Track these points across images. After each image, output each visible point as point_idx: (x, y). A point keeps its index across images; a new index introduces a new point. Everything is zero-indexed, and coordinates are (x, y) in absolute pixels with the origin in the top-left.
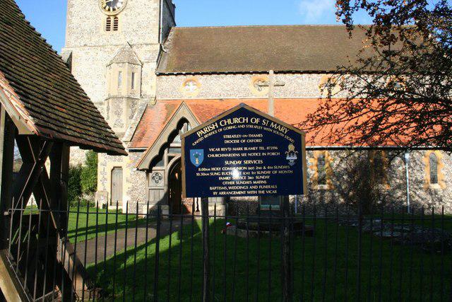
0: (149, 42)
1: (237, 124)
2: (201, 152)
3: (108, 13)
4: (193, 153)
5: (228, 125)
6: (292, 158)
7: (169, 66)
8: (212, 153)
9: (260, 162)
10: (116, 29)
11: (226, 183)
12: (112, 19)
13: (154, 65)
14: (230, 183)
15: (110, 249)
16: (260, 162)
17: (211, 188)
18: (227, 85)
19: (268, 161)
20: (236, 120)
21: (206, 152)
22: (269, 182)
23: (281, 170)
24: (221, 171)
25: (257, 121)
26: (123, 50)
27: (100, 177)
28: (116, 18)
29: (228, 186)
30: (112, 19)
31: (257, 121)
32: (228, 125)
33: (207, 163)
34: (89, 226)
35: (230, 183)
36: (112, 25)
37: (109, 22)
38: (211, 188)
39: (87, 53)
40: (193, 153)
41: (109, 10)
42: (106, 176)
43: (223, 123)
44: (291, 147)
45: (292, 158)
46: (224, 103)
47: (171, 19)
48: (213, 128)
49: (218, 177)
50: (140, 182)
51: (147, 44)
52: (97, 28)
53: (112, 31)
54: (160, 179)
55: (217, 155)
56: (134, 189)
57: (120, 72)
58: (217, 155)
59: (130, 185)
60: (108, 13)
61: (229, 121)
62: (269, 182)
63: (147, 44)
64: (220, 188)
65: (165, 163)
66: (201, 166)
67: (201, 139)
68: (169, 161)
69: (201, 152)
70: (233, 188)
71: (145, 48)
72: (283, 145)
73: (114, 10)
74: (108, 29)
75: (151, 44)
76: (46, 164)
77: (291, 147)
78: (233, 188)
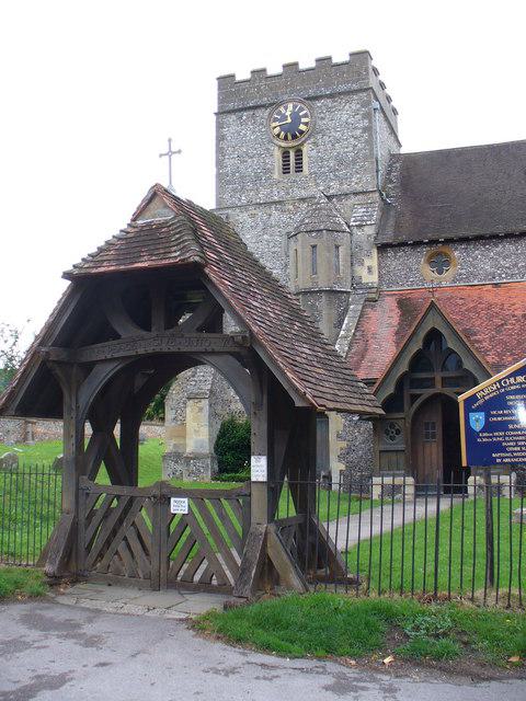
0: (359, 188)
1: (521, 384)
2: (481, 416)
3: (283, 144)
4: (473, 416)
5: (511, 385)
8: (494, 416)
10: (299, 169)
11: (511, 449)
12: (292, 154)
13: (370, 231)
14: (516, 449)
17: (494, 455)
21: (488, 416)
24: (505, 436)
28: (299, 153)
29: (512, 452)
30: (292, 154)
32: (511, 385)
34: (167, 157)
35: (516, 449)
36: (292, 161)
37: (286, 155)
38: (494, 455)
39: (253, 216)
40: (473, 416)
41: (286, 138)
43: (505, 382)
48: (495, 388)
49: (500, 442)
50: (360, 438)
54: (398, 432)
55: (499, 419)
56: (349, 450)
57: (314, 247)
58: (499, 419)
59: (344, 444)
60: (283, 144)
61: (512, 380)
64: (502, 455)
65: (406, 407)
67: (481, 402)
68: (412, 403)
69: (481, 416)
70: (519, 454)
71: (353, 200)
73: (294, 137)
74: (286, 170)
76: (47, 616)
78: (519, 454)
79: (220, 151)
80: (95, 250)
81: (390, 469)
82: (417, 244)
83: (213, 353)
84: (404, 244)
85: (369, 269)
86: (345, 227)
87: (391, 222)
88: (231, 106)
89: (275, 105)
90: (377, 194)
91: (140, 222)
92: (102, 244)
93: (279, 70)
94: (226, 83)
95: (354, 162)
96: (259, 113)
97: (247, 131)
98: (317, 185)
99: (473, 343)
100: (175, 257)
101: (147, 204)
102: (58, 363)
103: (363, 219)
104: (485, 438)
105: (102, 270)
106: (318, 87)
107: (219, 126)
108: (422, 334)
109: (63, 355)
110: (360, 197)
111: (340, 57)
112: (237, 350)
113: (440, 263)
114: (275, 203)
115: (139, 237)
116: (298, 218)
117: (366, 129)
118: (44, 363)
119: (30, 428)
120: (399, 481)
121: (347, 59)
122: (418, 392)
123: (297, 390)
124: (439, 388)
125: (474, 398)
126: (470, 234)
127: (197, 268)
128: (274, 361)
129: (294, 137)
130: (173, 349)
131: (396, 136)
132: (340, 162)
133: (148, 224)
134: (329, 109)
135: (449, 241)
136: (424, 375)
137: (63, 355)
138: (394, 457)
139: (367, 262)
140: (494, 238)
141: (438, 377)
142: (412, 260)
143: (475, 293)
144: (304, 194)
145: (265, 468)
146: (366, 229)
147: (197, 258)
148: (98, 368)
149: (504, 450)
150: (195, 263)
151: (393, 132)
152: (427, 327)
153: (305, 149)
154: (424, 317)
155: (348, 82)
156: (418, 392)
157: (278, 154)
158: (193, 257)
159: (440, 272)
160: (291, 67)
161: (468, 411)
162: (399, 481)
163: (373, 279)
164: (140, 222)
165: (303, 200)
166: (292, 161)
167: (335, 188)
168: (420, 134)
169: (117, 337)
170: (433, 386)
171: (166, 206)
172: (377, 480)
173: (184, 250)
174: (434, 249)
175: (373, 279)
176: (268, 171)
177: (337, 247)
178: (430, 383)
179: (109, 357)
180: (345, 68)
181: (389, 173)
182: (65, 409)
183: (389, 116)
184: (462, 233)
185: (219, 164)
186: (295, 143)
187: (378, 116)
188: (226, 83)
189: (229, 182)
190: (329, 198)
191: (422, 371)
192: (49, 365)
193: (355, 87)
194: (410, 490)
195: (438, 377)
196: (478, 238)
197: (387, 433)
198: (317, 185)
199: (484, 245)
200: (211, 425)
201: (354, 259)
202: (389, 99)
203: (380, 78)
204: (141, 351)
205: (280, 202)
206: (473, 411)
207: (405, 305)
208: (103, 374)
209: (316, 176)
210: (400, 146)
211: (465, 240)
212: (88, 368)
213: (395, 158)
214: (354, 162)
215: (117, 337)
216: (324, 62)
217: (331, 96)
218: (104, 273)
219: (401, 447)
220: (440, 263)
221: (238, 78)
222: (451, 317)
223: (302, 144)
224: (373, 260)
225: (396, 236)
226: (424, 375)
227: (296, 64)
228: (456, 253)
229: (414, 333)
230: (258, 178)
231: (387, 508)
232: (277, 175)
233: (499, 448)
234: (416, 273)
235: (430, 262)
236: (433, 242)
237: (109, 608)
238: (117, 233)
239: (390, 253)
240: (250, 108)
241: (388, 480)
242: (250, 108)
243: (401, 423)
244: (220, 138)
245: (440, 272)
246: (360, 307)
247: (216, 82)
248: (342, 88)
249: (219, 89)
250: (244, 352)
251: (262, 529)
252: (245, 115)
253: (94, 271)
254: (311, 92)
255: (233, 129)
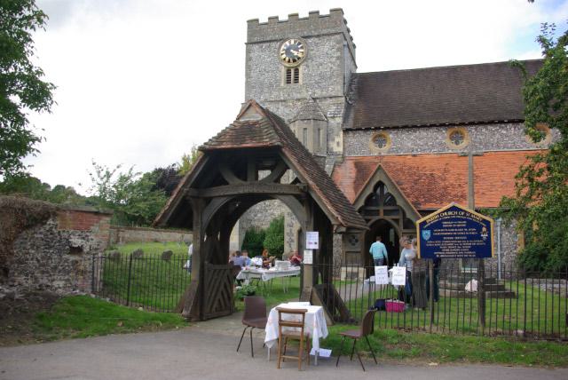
2: (428, 232)
3: (288, 65)
4: (424, 232)
6: (484, 236)
7: (356, 120)
9: (465, 238)
10: (296, 80)
12: (293, 71)
13: (339, 120)
15: (353, 295)
16: (465, 238)
18: (420, 139)
19: (470, 238)
20: (450, 213)
22: (470, 250)
23: (479, 243)
25: (463, 213)
26: (306, 108)
27: (287, 238)
28: (297, 71)
30: (293, 71)
31: (463, 213)
33: (433, 238)
36: (292, 76)
37: (289, 72)
40: (424, 232)
41: (289, 61)
42: (293, 238)
44: (484, 229)
45: (484, 236)
46: (417, 159)
47: (352, 63)
51: (331, 98)
52: (277, 81)
53: (292, 85)
54: (357, 241)
57: (305, 129)
62: (470, 250)
63: (331, 98)
66: (430, 240)
69: (428, 232)
71: (329, 101)
72: (479, 228)
73: (294, 61)
74: (288, 82)
75: (335, 97)
77: (484, 229)
79: (248, 68)
80: (216, 135)
81: (352, 263)
82: (367, 129)
83: (283, 194)
84: (360, 129)
85: (338, 143)
86: (324, 118)
87: (352, 115)
88: (256, 39)
89: (282, 40)
90: (344, 99)
91: (241, 120)
92: (220, 131)
93: (286, 18)
94: (253, 24)
95: (330, 78)
96: (273, 44)
97: (263, 55)
98: (307, 91)
99: (402, 189)
100: (266, 142)
101: (246, 111)
102: (193, 197)
103: (334, 112)
104: (430, 244)
105: (223, 147)
106: (310, 30)
107: (248, 52)
108: (373, 184)
109: (194, 192)
110: (334, 99)
111: (325, 11)
112: (298, 193)
113: (380, 141)
114: (282, 101)
115: (241, 129)
116: (295, 111)
117: (338, 58)
118: (184, 197)
119: (121, 234)
120: (355, 270)
121: (328, 13)
122: (369, 217)
123: (333, 216)
124: (381, 216)
125: (425, 223)
126: (400, 125)
127: (278, 148)
128: (320, 199)
129: (294, 61)
130: (261, 191)
131: (355, 62)
132: (322, 76)
133: (247, 122)
134: (317, 45)
135: (386, 128)
136: (373, 208)
137: (194, 192)
138: (354, 255)
139: (337, 140)
140: (415, 127)
141: (381, 209)
142: (364, 139)
143: (401, 160)
144: (299, 96)
145: (311, 257)
146: (337, 119)
147: (279, 143)
148: (214, 200)
149: (441, 250)
150: (278, 146)
151: (353, 59)
152: (376, 180)
153: (301, 69)
154: (375, 174)
155: (328, 28)
156: (369, 217)
157: (284, 71)
158: (276, 142)
159: (380, 146)
160: (294, 16)
161: (421, 229)
162: (355, 270)
163: (340, 149)
164: (241, 120)
165: (299, 100)
166: (292, 76)
167: (318, 93)
168: (367, 63)
169: (227, 183)
170: (378, 214)
171: (257, 112)
172: (343, 269)
173: (271, 138)
174: (378, 132)
175: (340, 149)
176: (277, 81)
177: (319, 130)
178: (377, 212)
179: (222, 194)
180: (327, 19)
181: (350, 85)
182: (194, 225)
183: (350, 47)
184: (395, 124)
185: (248, 75)
186: (295, 65)
187: (346, 49)
188: (253, 24)
189: (253, 87)
190: (314, 99)
191: (371, 205)
192: (188, 198)
193: (333, 31)
194: (361, 275)
195: (381, 209)
196: (404, 127)
197: (350, 241)
198: (307, 91)
199: (408, 131)
200: (240, 235)
201: (328, 138)
202: (351, 39)
203: (348, 25)
204: (241, 192)
205: (284, 101)
206: (425, 229)
207: (360, 166)
208: (217, 204)
209: (307, 86)
210: (356, 67)
211: (396, 128)
212: (208, 200)
213: (354, 75)
214: (330, 78)
215: (227, 183)
216: (314, 14)
217: (318, 36)
218: (224, 149)
219: (359, 250)
220: (380, 141)
221: (260, 22)
222: (390, 175)
223: (299, 66)
224: (340, 138)
225: (355, 124)
226: (373, 208)
227: (297, 15)
228: (391, 136)
229: (369, 183)
230: (271, 85)
231: (348, 285)
232: (283, 84)
233: (438, 249)
234: (367, 147)
235: (375, 140)
236: (377, 129)
237: (225, 333)
238: (228, 126)
239: (351, 134)
240: (267, 41)
241: (349, 269)
242: (267, 41)
243: (359, 235)
244: (248, 59)
245: (380, 146)
246: (332, 167)
247: (246, 24)
248: (325, 31)
249: (248, 28)
250: (303, 194)
251: (310, 290)
252: (264, 45)
253: (218, 147)
254: (305, 34)
255: (257, 54)
